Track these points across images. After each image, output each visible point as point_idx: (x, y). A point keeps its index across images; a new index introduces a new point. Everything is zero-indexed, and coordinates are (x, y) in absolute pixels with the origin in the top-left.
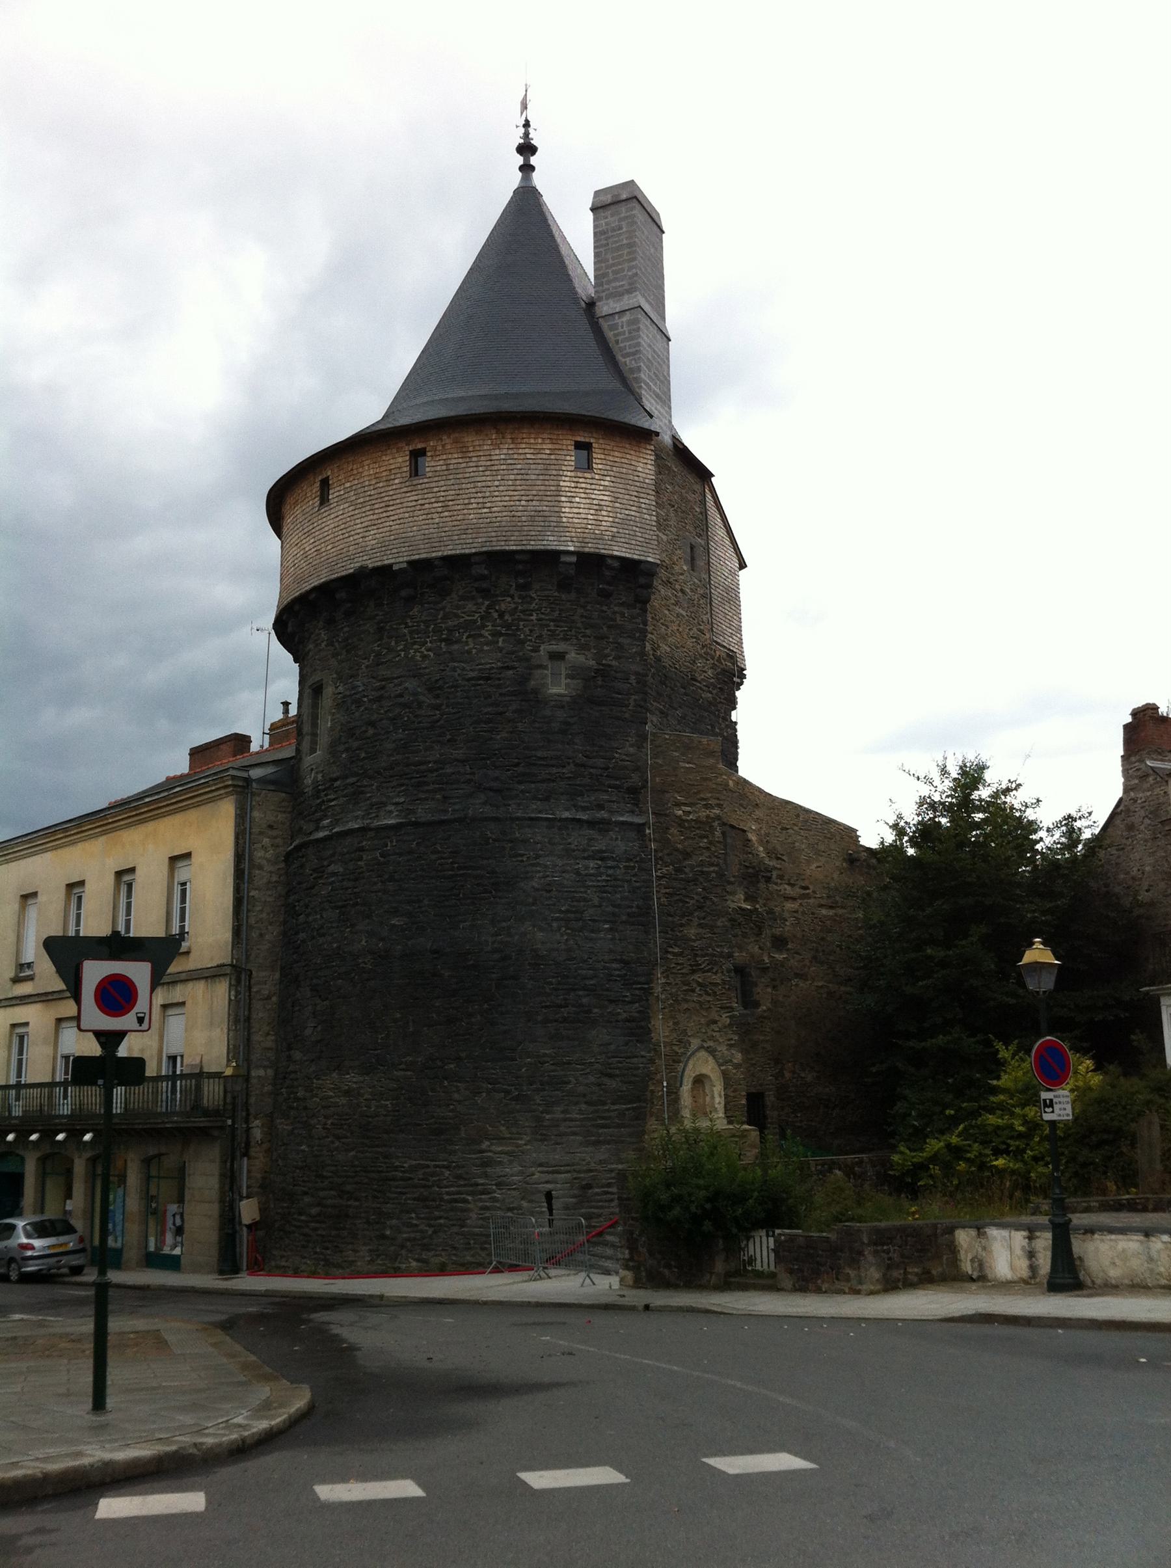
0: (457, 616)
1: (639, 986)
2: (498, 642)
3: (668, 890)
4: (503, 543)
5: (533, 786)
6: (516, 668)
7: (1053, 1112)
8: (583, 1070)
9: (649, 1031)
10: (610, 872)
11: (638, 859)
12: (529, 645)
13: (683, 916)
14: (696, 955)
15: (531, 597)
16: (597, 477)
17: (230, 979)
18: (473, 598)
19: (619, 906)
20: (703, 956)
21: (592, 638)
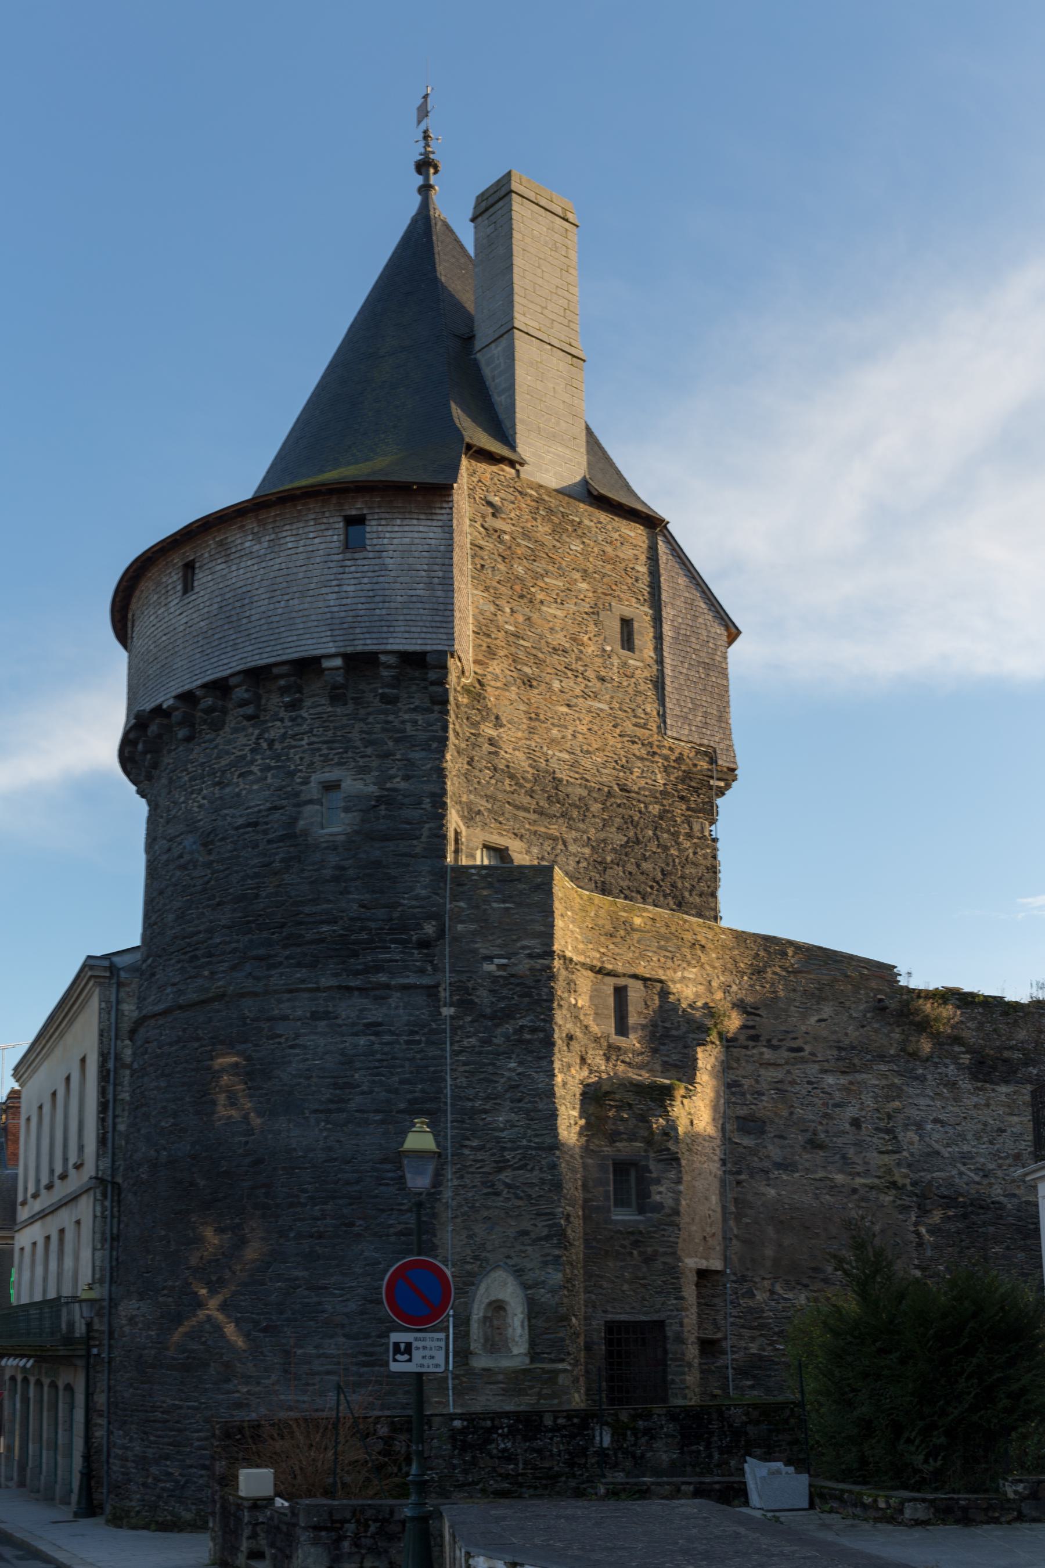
0: (228, 753)
2: (266, 778)
3: (467, 1068)
4: (257, 657)
5: (299, 950)
6: (282, 808)
7: (410, 1360)
8: (341, 1296)
10: (386, 1049)
11: (426, 1030)
12: (300, 777)
13: (488, 1098)
14: (504, 1149)
15: (303, 718)
16: (371, 555)
17: (95, 1193)
18: (244, 729)
21: (374, 758)
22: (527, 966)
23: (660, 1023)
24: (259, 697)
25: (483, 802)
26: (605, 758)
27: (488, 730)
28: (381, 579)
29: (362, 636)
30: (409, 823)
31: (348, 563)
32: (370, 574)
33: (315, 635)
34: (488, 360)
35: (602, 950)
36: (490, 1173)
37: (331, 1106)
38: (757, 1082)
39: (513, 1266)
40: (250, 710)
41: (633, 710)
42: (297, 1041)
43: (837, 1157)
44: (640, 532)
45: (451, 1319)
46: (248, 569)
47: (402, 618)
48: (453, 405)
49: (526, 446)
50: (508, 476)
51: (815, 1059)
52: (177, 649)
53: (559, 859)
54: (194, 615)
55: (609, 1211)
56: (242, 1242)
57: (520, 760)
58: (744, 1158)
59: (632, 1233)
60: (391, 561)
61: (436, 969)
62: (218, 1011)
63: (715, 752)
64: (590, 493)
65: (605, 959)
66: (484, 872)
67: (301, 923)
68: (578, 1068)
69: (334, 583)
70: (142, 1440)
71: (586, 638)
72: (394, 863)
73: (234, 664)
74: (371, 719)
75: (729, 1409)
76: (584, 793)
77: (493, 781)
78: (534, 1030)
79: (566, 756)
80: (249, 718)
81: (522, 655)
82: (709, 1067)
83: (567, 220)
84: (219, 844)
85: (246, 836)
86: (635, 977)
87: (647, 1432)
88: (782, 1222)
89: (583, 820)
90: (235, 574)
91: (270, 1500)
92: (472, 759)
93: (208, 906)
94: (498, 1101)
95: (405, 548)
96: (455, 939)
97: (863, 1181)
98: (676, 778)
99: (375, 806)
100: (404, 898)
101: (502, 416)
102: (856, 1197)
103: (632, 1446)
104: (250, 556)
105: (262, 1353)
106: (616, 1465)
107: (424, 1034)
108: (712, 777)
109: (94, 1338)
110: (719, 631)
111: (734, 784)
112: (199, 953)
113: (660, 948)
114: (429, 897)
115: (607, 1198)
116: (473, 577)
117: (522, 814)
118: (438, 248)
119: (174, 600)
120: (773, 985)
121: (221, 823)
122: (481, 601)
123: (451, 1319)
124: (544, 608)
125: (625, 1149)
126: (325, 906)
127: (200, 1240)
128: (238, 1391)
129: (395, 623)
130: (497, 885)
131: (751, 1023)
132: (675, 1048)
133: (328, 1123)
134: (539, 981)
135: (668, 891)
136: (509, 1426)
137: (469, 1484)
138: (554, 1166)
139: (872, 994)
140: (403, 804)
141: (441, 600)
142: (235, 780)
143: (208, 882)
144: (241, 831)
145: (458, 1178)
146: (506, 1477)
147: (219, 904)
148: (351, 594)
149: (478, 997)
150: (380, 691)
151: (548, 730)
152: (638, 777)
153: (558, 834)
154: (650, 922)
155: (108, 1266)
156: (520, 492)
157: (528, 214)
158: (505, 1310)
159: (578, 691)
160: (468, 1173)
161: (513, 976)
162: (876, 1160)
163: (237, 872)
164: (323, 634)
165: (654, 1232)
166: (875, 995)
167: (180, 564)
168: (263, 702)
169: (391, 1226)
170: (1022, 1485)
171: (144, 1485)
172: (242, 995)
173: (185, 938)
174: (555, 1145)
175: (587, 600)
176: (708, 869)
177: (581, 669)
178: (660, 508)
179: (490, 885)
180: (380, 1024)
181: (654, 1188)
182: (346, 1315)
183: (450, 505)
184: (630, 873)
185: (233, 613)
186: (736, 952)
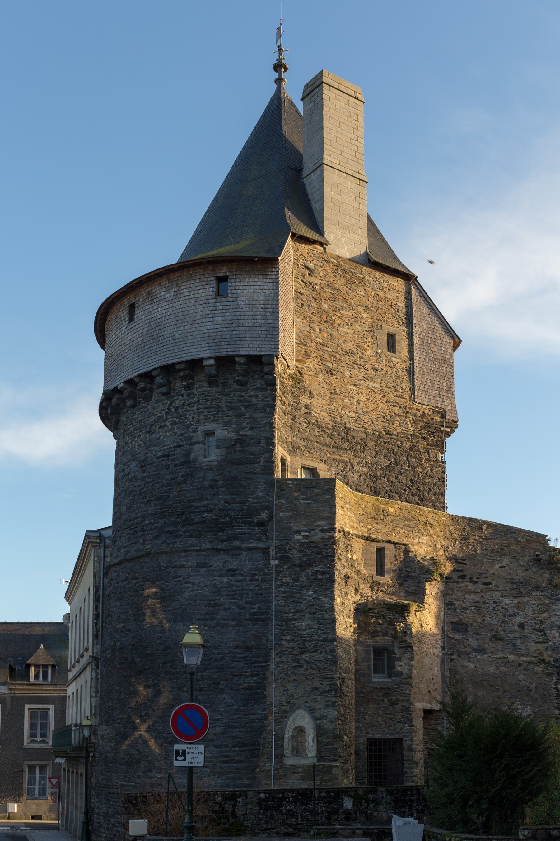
0: (153, 414)
1: (258, 664)
2: (174, 428)
3: (285, 595)
4: (167, 359)
6: (183, 446)
7: (185, 760)
9: (265, 697)
10: (239, 584)
11: (261, 573)
12: (192, 428)
13: (296, 612)
15: (194, 394)
16: (231, 299)
17: (92, 665)
18: (162, 401)
19: (244, 608)
20: (310, 641)
21: (233, 417)
22: (320, 537)
23: (404, 569)
24: (169, 382)
25: (302, 442)
26: (377, 416)
27: (305, 400)
28: (237, 313)
29: (225, 347)
30: (253, 455)
31: (218, 304)
32: (230, 311)
33: (199, 346)
34: (309, 182)
35: (369, 527)
36: (297, 655)
37: (207, 617)
38: (464, 602)
39: (309, 707)
40: (164, 390)
41: (395, 387)
42: (189, 580)
43: (510, 645)
44: (400, 283)
45: (274, 737)
46: (163, 308)
47: (248, 336)
48: (286, 210)
49: (329, 233)
50: (319, 251)
51: (498, 589)
52: (125, 355)
53: (348, 474)
54: (135, 335)
55: (370, 676)
56: (158, 693)
57: (325, 417)
58: (455, 646)
59: (384, 689)
60: (243, 303)
61: (267, 538)
62: (146, 563)
63: (445, 411)
64: (369, 260)
65: (371, 532)
66: (296, 482)
67: (192, 512)
68: (353, 594)
69: (210, 316)
70: (107, 804)
71: (366, 346)
72: (244, 478)
73: (155, 363)
74: (232, 395)
75: (424, 788)
76: (364, 436)
77: (308, 430)
78: (323, 573)
79: (353, 414)
80: (164, 394)
81: (326, 356)
82: (433, 594)
83: (357, 99)
84: (148, 467)
85: (163, 462)
86: (389, 542)
87: (374, 801)
88: (477, 682)
89: (363, 452)
90: (156, 311)
91: (146, 835)
92: (295, 417)
93: (143, 503)
94: (302, 614)
95: (251, 295)
96: (279, 521)
97: (525, 659)
98: (421, 427)
99: (234, 445)
100: (250, 498)
101: (316, 216)
102: (521, 668)
103: (365, 808)
104: (164, 301)
105: (168, 755)
106: (355, 819)
107: (260, 576)
108: (443, 426)
109: (91, 747)
110: (448, 341)
111: (456, 430)
112: (138, 529)
113: (405, 525)
114: (264, 497)
115: (369, 669)
116: (296, 311)
117: (325, 448)
118: (285, 116)
119: (124, 326)
120: (474, 546)
121: (149, 455)
122: (301, 325)
123: (274, 737)
124: (340, 329)
125: (380, 641)
126: (206, 502)
127: (136, 692)
128: (156, 777)
129: (244, 339)
130: (303, 490)
131: (460, 569)
132: (413, 583)
133: (205, 626)
134: (327, 545)
135: (415, 493)
136: (292, 797)
137: (269, 829)
138: (333, 651)
139: (532, 552)
140: (249, 444)
141: (271, 325)
142: (157, 430)
143: (143, 489)
144: (160, 459)
145: (278, 658)
146: (290, 825)
147: (148, 501)
148: (220, 322)
149: (292, 554)
150: (237, 378)
151: (342, 399)
152: (397, 426)
153: (348, 460)
154: (399, 511)
155: (98, 706)
156: (326, 261)
157: (333, 96)
158: (305, 732)
159: (360, 377)
160: (284, 654)
161: (312, 542)
162: (533, 647)
163: (158, 483)
164: (203, 346)
165: (397, 688)
166: (534, 552)
167: (127, 305)
168: (172, 385)
169: (240, 684)
170: (527, 831)
171: (107, 829)
172: (159, 554)
173: (130, 521)
174: (333, 638)
175: (367, 323)
176: (439, 479)
177: (363, 364)
178: (414, 269)
179: (299, 490)
180: (235, 570)
181: (397, 663)
182: (215, 734)
183: (277, 269)
184: (392, 482)
185: (155, 333)
186: (452, 528)
